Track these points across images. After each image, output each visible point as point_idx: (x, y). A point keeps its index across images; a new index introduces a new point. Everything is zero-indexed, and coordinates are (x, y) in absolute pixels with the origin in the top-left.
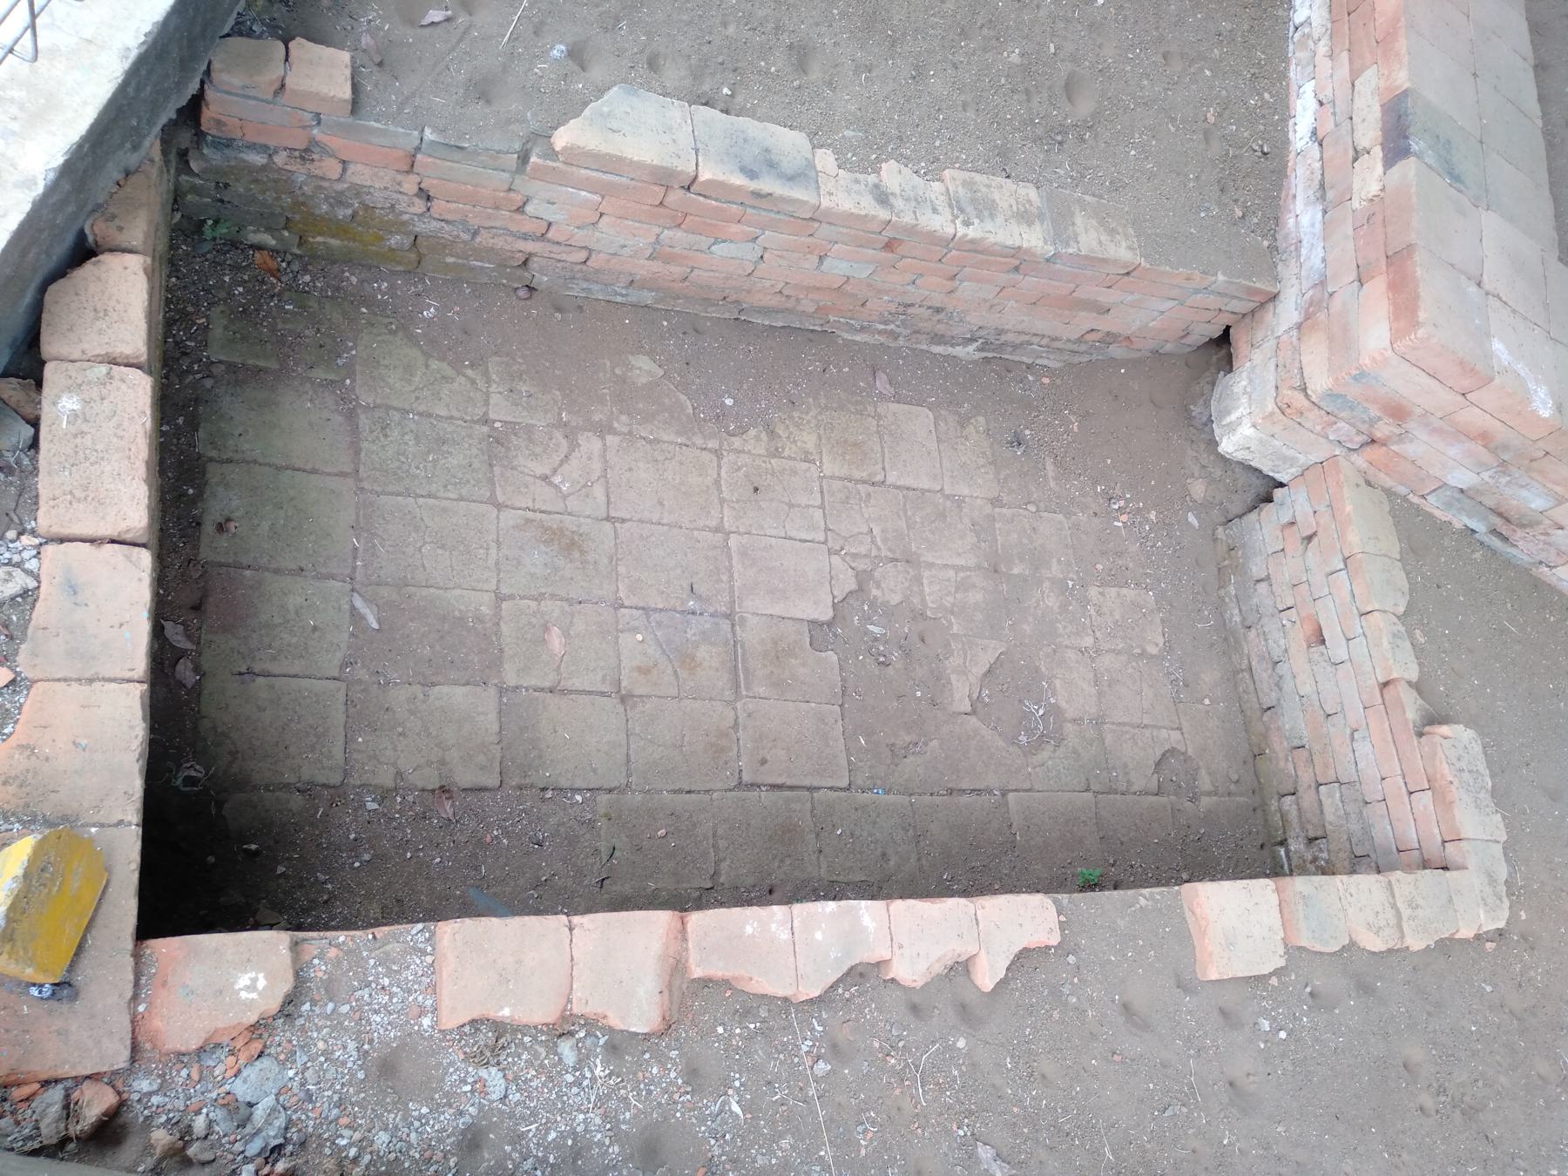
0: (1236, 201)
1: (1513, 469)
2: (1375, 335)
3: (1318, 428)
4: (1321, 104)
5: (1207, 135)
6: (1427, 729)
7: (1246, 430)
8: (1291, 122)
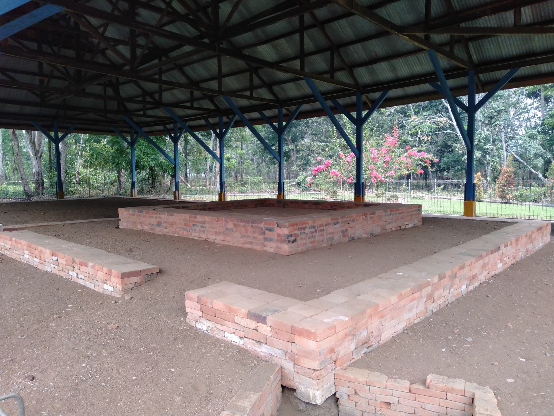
2: (311, 345)
4: (234, 333)
6: (427, 385)
7: (318, 393)
8: (233, 342)
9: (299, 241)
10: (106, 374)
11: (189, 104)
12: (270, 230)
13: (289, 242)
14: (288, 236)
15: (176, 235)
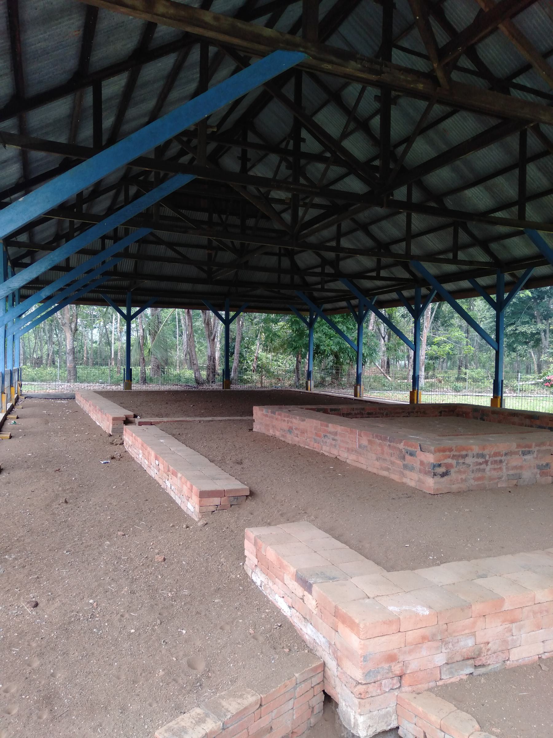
0: (283, 648)
1: (447, 639)
3: (379, 691)
4: (283, 597)
5: (255, 638)
7: (361, 719)
9: (453, 475)
10: (108, 617)
11: (374, 274)
12: (411, 454)
13: (435, 475)
14: (434, 466)
15: (306, 447)
